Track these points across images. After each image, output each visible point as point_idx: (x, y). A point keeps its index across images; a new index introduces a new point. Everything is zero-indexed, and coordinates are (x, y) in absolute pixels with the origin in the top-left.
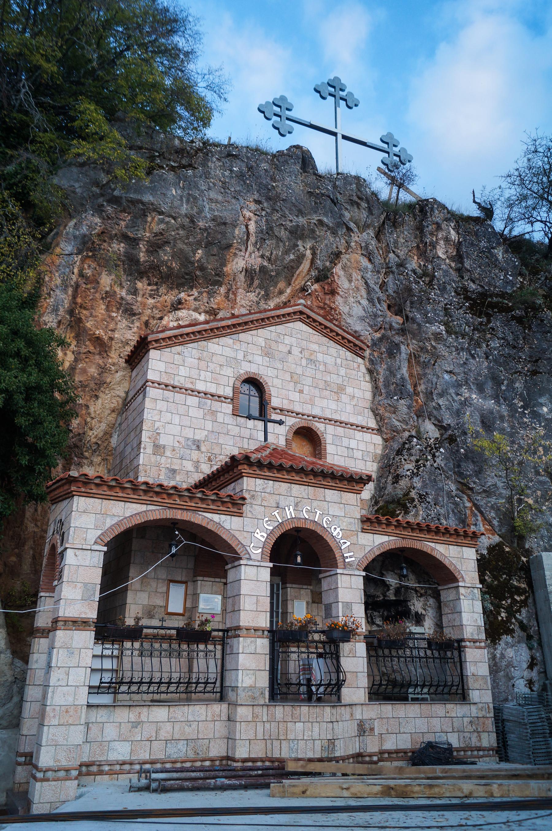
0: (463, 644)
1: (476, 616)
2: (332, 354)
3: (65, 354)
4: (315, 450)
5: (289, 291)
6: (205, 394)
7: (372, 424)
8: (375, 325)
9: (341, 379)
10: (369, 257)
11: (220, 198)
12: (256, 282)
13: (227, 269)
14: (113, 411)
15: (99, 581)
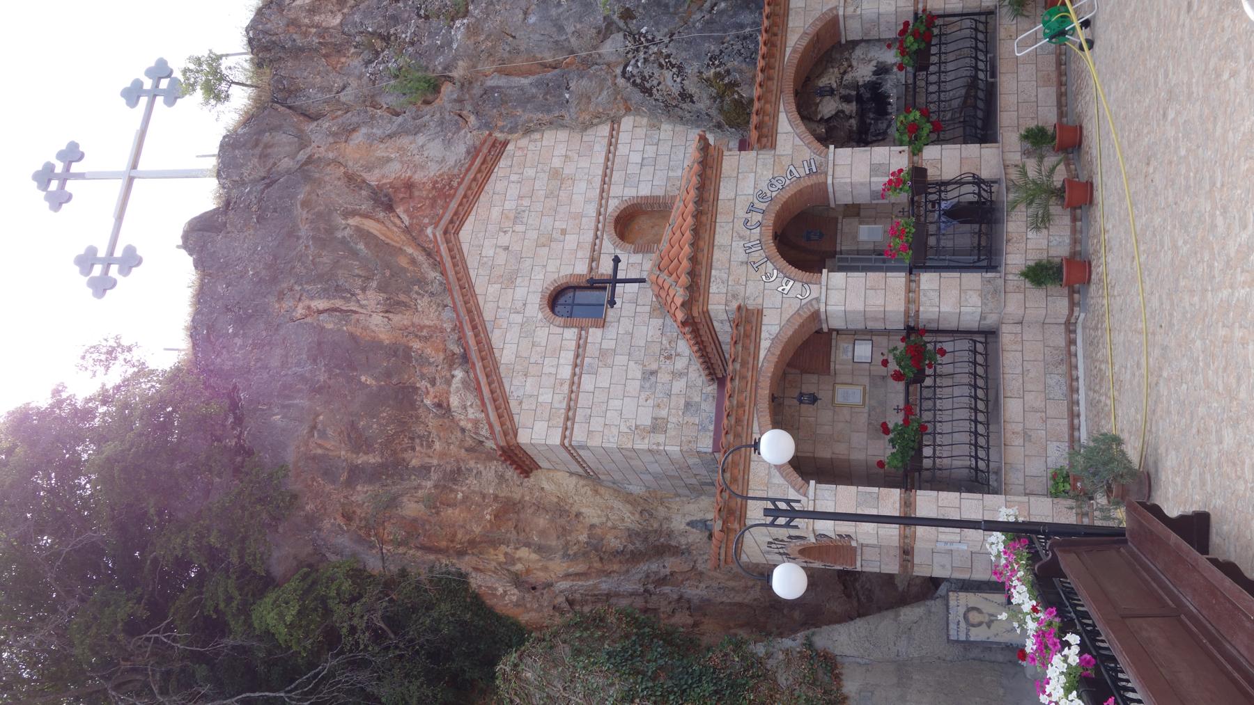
0: (920, 12)
2: (508, 186)
3: (520, 559)
4: (645, 213)
5: (410, 250)
6: (576, 365)
7: (605, 130)
8: (457, 123)
9: (542, 175)
10: (350, 130)
11: (279, 351)
12: (402, 297)
13: (385, 337)
15: (853, 488)
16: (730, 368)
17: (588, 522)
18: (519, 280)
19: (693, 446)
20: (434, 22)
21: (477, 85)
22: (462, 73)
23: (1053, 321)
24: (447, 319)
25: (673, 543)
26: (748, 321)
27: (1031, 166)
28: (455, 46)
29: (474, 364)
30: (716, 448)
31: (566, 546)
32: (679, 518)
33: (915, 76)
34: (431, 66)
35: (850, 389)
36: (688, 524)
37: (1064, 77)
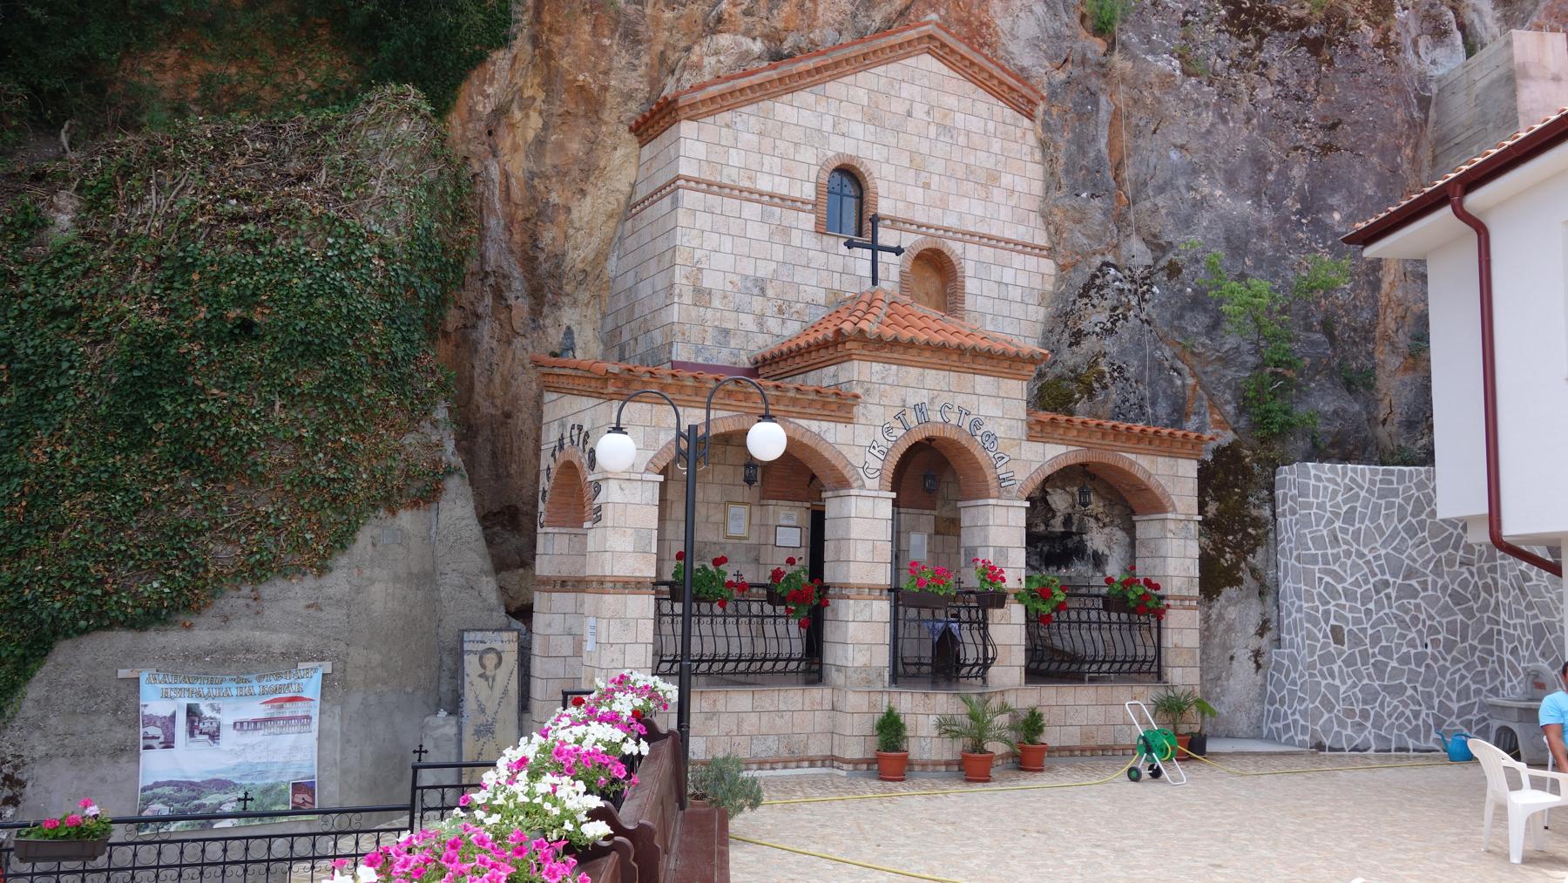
0: (1165, 602)
1: (1188, 562)
3: (527, 116)
4: (944, 285)
6: (771, 197)
7: (1041, 239)
8: (1057, 56)
9: (992, 160)
14: (611, 216)
16: (770, 383)
17: (574, 205)
18: (872, 128)
19: (679, 338)
20: (1178, 33)
21: (1101, 83)
22: (1118, 66)
23: (836, 742)
24: (824, 34)
25: (546, 310)
26: (840, 407)
27: (1003, 720)
28: (1149, 58)
29: (775, 68)
30: (674, 365)
31: (544, 176)
32: (576, 317)
33: (1097, 596)
34: (1126, 26)
35: (744, 522)
36: (569, 328)
37: (1093, 753)
